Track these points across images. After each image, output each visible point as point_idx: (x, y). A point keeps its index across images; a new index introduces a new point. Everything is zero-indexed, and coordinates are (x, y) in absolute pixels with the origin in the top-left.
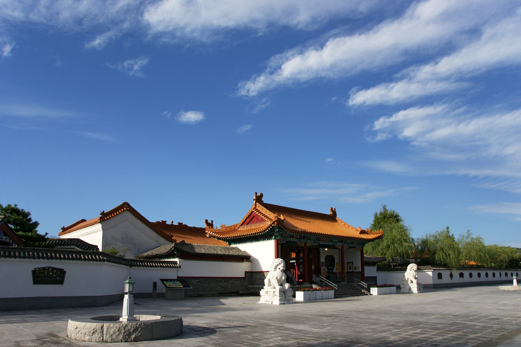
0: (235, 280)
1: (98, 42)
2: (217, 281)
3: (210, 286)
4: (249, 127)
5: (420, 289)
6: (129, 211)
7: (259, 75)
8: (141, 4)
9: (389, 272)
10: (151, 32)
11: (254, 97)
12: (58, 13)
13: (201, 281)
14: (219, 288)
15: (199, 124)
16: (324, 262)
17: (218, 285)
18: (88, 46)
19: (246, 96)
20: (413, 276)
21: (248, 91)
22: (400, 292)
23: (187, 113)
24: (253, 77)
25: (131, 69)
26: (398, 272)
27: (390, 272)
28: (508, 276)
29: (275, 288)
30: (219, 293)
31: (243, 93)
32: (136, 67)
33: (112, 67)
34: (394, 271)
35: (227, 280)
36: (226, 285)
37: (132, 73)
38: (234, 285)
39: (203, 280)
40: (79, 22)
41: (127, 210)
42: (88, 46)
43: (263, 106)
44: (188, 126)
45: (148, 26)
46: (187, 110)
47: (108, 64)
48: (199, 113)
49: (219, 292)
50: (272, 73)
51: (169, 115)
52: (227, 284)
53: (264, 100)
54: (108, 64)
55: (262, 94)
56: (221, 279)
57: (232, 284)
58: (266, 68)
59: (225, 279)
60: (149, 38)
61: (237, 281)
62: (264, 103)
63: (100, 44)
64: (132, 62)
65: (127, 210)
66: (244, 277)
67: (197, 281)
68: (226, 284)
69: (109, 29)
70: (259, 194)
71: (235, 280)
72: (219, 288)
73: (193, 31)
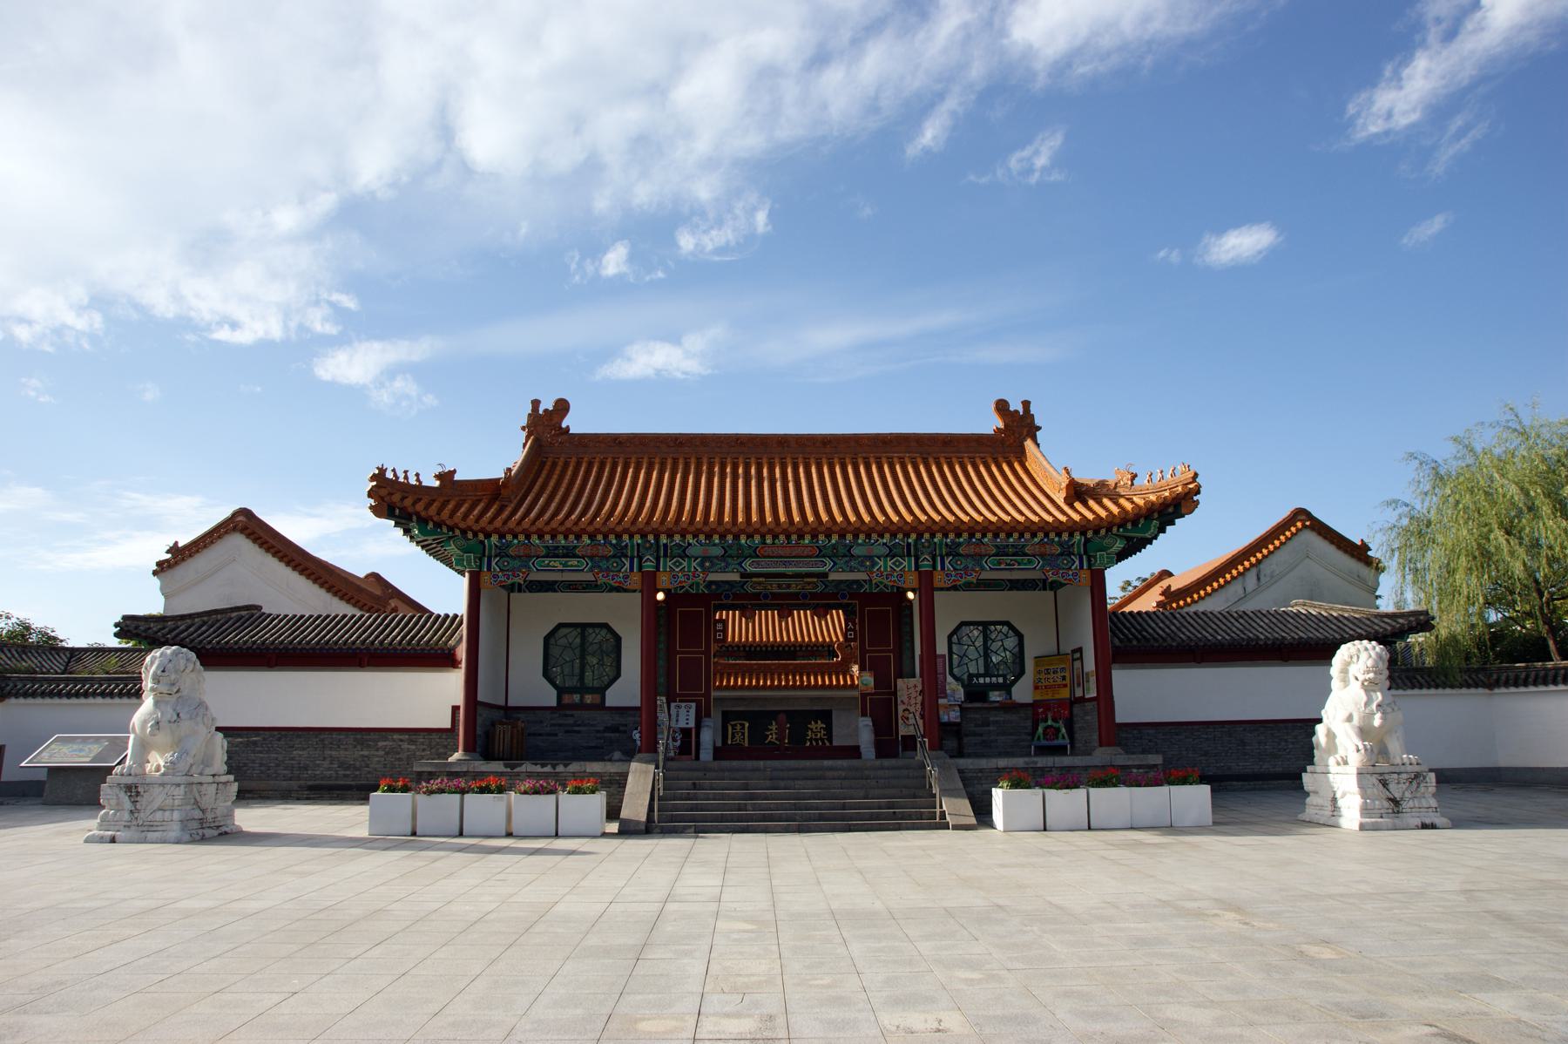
0: (401, 740)
1: (931, 133)
2: (323, 740)
3: (292, 759)
4: (1437, 224)
5: (1395, 802)
6: (1312, 528)
7: (1407, 59)
8: (994, 9)
9: (1496, 691)
10: (1039, 66)
11: (1413, 126)
12: (824, 106)
13: (255, 743)
14: (329, 769)
15: (1269, 260)
16: (945, 655)
17: (324, 759)
18: (912, 151)
19: (1387, 133)
20: (1350, 719)
21: (1389, 115)
22: (1301, 817)
23: (1224, 239)
24: (1388, 73)
25: (1030, 171)
26: (1471, 694)
27: (1503, 690)
28: (3, 744)
29: (1346, 763)
30: (311, 788)
31: (1373, 129)
32: (1041, 161)
33: (984, 180)
34: (1526, 684)
35: (365, 737)
36: (363, 756)
37: (1034, 179)
38: (400, 759)
39: (264, 739)
40: (872, 107)
41: (1304, 526)
42: (912, 151)
43: (1463, 141)
44: (1239, 271)
45: (1029, 53)
46: (1221, 229)
47: (972, 178)
48: (1255, 228)
49: (310, 783)
50: (1451, 35)
51: (1175, 257)
52: (365, 753)
53: (1458, 122)
54: (972, 178)
55: (1440, 111)
56: (342, 737)
57: (387, 753)
58: (1418, 27)
59: (359, 736)
60: (1041, 82)
61: (411, 742)
62: (1462, 133)
63: (935, 138)
64: (1026, 153)
65: (1304, 526)
66: (449, 726)
67: (241, 743)
68: (362, 753)
69: (941, 96)
70: (547, 404)
71: (401, 740)
72: (329, 769)
73: (1146, 18)
